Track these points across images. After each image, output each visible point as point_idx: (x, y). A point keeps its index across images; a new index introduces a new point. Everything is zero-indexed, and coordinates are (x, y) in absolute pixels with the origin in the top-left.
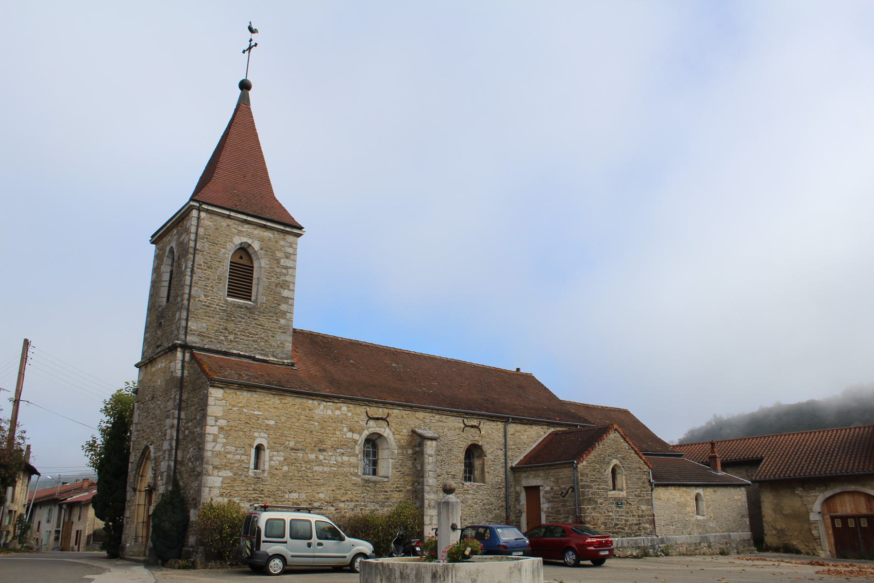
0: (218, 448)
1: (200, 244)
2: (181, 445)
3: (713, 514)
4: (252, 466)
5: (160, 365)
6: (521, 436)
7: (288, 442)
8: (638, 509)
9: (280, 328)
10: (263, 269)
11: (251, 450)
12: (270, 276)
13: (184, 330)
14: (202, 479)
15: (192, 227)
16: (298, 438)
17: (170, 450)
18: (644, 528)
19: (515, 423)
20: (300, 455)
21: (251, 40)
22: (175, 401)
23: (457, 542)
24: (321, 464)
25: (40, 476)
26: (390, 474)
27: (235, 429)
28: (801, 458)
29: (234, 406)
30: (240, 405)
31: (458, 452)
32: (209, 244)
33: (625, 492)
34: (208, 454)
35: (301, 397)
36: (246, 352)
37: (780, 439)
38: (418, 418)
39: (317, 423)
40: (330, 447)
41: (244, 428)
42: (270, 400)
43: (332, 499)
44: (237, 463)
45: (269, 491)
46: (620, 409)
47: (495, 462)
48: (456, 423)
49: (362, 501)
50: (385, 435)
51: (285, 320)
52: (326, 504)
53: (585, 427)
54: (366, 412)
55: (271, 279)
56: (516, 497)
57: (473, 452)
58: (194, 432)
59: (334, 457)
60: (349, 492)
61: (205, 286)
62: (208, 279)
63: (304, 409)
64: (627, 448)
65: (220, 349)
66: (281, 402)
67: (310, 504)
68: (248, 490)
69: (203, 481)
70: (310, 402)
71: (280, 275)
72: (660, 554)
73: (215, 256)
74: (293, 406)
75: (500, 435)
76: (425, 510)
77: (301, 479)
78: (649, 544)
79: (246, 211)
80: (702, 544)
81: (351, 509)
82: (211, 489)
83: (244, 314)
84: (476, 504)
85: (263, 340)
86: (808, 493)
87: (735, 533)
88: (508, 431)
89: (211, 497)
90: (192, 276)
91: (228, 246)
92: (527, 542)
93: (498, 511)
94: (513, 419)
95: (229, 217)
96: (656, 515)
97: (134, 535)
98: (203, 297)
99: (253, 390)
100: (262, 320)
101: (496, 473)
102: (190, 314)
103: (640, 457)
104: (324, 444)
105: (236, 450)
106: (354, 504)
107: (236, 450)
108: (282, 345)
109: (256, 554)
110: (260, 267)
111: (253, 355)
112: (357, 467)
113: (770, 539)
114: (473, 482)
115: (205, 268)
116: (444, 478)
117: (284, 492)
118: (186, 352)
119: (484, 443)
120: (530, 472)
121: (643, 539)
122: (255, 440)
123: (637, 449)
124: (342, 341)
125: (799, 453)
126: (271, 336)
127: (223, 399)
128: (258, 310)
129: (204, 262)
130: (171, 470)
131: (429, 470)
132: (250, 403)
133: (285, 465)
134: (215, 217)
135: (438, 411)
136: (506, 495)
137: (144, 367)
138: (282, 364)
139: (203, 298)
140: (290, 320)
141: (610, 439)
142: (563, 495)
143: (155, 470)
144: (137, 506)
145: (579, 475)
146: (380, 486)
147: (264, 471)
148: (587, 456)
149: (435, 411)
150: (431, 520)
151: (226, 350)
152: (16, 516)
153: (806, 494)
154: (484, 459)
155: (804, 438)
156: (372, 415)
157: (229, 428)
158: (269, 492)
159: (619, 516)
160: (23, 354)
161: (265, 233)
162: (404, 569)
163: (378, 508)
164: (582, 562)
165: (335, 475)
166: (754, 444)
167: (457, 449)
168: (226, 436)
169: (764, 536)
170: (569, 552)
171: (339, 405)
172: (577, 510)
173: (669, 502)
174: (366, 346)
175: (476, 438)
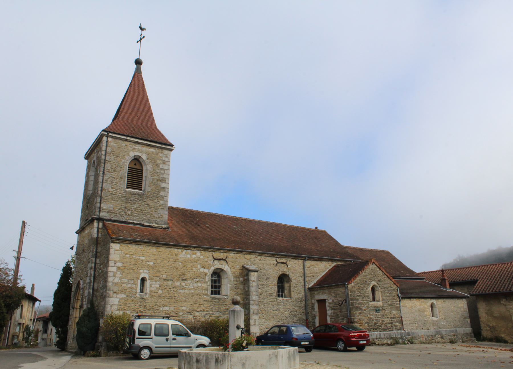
0: (117, 280)
1: (109, 157)
2: (97, 279)
3: (444, 316)
4: (139, 291)
5: (87, 231)
6: (315, 269)
7: (162, 276)
8: (391, 313)
9: (160, 206)
10: (149, 171)
11: (138, 281)
12: (153, 175)
13: (99, 209)
16: (169, 272)
17: (90, 283)
18: (395, 326)
19: (311, 260)
20: (170, 283)
21: (141, 35)
22: (93, 252)
24: (183, 288)
25: (41, 302)
27: (128, 268)
28: (504, 279)
29: (127, 254)
30: (130, 253)
31: (273, 279)
32: (114, 157)
33: (381, 302)
34: (110, 284)
35: (170, 248)
36: (138, 221)
37: (489, 267)
38: (246, 259)
39: (181, 263)
40: (189, 278)
41: (133, 268)
43: (191, 310)
44: (128, 289)
45: (149, 306)
46: (383, 251)
47: (297, 284)
50: (225, 269)
51: (163, 201)
52: (187, 313)
53: (355, 262)
54: (213, 255)
55: (154, 177)
56: (312, 306)
57: (283, 279)
58: (103, 271)
59: (192, 284)
60: (202, 306)
61: (112, 182)
62: (114, 178)
63: (172, 255)
64: (382, 274)
65: (121, 220)
66: (157, 251)
67: (176, 314)
69: (106, 301)
70: (176, 250)
71: (160, 174)
72: (407, 342)
73: (118, 164)
74: (165, 253)
75: (301, 268)
76: (251, 316)
77: (171, 298)
78: (399, 336)
79: (137, 136)
80: (437, 336)
81: (203, 316)
82: (112, 306)
83: (137, 199)
84: (286, 312)
85: (149, 214)
86: (510, 303)
87: (460, 329)
88: (305, 265)
90: (103, 177)
91: (126, 158)
92: (312, 335)
93: (300, 316)
94: (308, 257)
95: (126, 140)
96: (403, 317)
97: (73, 336)
98: (111, 189)
100: (149, 201)
101: (298, 291)
102: (102, 199)
103: (391, 280)
104: (186, 276)
105: (128, 281)
107: (128, 281)
108: (161, 217)
109: (132, 347)
110: (147, 170)
111: (142, 223)
113: (485, 333)
114: (284, 297)
115: (112, 171)
116: (264, 296)
117: (159, 307)
118: (100, 222)
119: (290, 273)
120: (320, 291)
121: (395, 333)
122: (140, 274)
123: (388, 275)
124: (203, 213)
125: (502, 276)
127: (120, 250)
129: (111, 168)
130: (90, 295)
131: (253, 290)
132: (137, 252)
133: (160, 290)
135: (259, 254)
136: (305, 305)
137: (80, 233)
138: (161, 228)
139: (110, 189)
140: (167, 201)
141: (369, 269)
142: (340, 305)
144: (74, 318)
145: (349, 292)
146: (222, 301)
147: (146, 294)
148: (354, 280)
150: (255, 322)
151: (125, 220)
152: (24, 326)
153: (508, 303)
154: (290, 283)
155: (507, 266)
156: (216, 257)
157: (124, 268)
158: (150, 307)
159: (378, 318)
160: (22, 230)
161: (150, 149)
163: (221, 315)
164: (348, 348)
165: (193, 295)
166: (472, 271)
169: (481, 330)
170: (340, 342)
171: (195, 252)
172: (349, 314)
173: (412, 309)
174: (218, 216)
175: (285, 270)
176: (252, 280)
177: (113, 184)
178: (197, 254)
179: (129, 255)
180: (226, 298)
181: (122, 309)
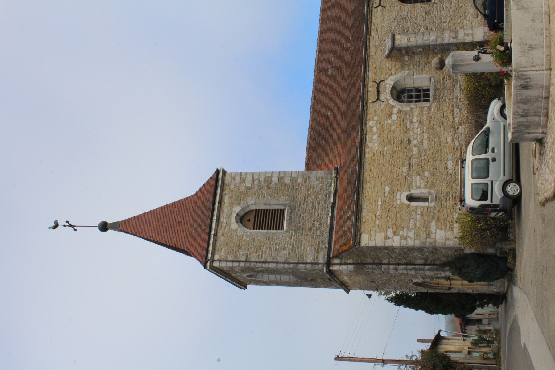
0: (411, 234)
1: (241, 257)
2: (411, 260)
4: (426, 204)
5: (345, 279)
7: (404, 174)
9: (305, 182)
10: (257, 201)
12: (262, 194)
13: (315, 265)
14: (439, 247)
15: (228, 266)
16: (399, 164)
17: (416, 270)
20: (414, 161)
21: (64, 226)
22: (374, 269)
23: (491, 56)
25: (441, 330)
26: (428, 76)
27: (394, 221)
29: (375, 223)
30: (374, 218)
34: (417, 243)
38: (376, 53)
39: (386, 148)
40: (406, 135)
41: (394, 213)
42: (368, 192)
43: (452, 129)
45: (447, 188)
48: (378, 16)
49: (452, 101)
50: (392, 83)
52: (456, 135)
55: (264, 194)
59: (414, 130)
60: (445, 114)
61: (276, 250)
62: (270, 248)
63: (374, 161)
65: (328, 234)
66: (369, 182)
67: (457, 150)
68: (446, 207)
71: (260, 185)
76: (459, 41)
79: (209, 220)
81: (460, 111)
82: (447, 239)
83: (297, 215)
85: (317, 197)
89: (454, 238)
90: (269, 263)
91: (240, 234)
95: (216, 235)
97: (487, 287)
98: (285, 251)
99: (360, 208)
100: (300, 198)
102: (300, 262)
105: (413, 219)
106: (455, 108)
107: (413, 219)
108: (320, 179)
109: (503, 208)
110: (255, 204)
112: (422, 109)
115: (261, 251)
117: (447, 174)
118: (332, 262)
122: (403, 203)
124: (312, 121)
126: (313, 190)
127: (370, 233)
128: (292, 203)
129: (256, 253)
130: (432, 268)
131: (422, 40)
132: (371, 210)
133: (424, 174)
134: (218, 247)
135: (368, 33)
137: (348, 287)
138: (336, 179)
139: (286, 252)
140: (298, 173)
143: (433, 278)
144: (463, 286)
147: (430, 193)
149: (368, 37)
151: (328, 228)
152: (472, 347)
156: (375, 97)
157: (394, 226)
158: (448, 187)
161: (226, 203)
162: (518, 115)
163: (459, 85)
165: (430, 128)
167: (401, 12)
168: (402, 229)
171: (368, 129)
176: (407, 42)
177: (278, 249)
178: (372, 125)
179: (377, 220)
180: (433, 80)
181: (451, 225)
